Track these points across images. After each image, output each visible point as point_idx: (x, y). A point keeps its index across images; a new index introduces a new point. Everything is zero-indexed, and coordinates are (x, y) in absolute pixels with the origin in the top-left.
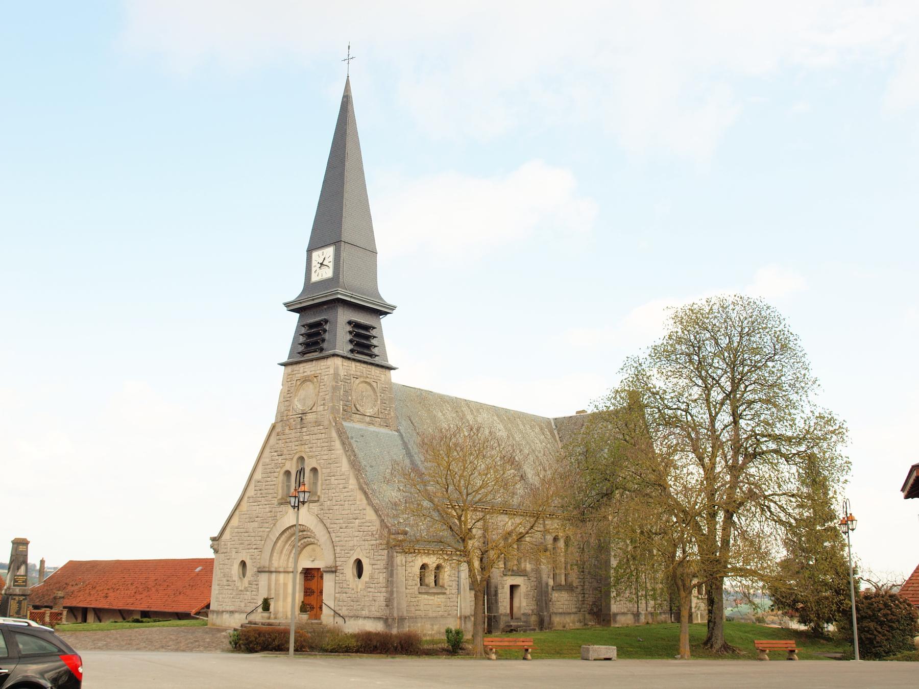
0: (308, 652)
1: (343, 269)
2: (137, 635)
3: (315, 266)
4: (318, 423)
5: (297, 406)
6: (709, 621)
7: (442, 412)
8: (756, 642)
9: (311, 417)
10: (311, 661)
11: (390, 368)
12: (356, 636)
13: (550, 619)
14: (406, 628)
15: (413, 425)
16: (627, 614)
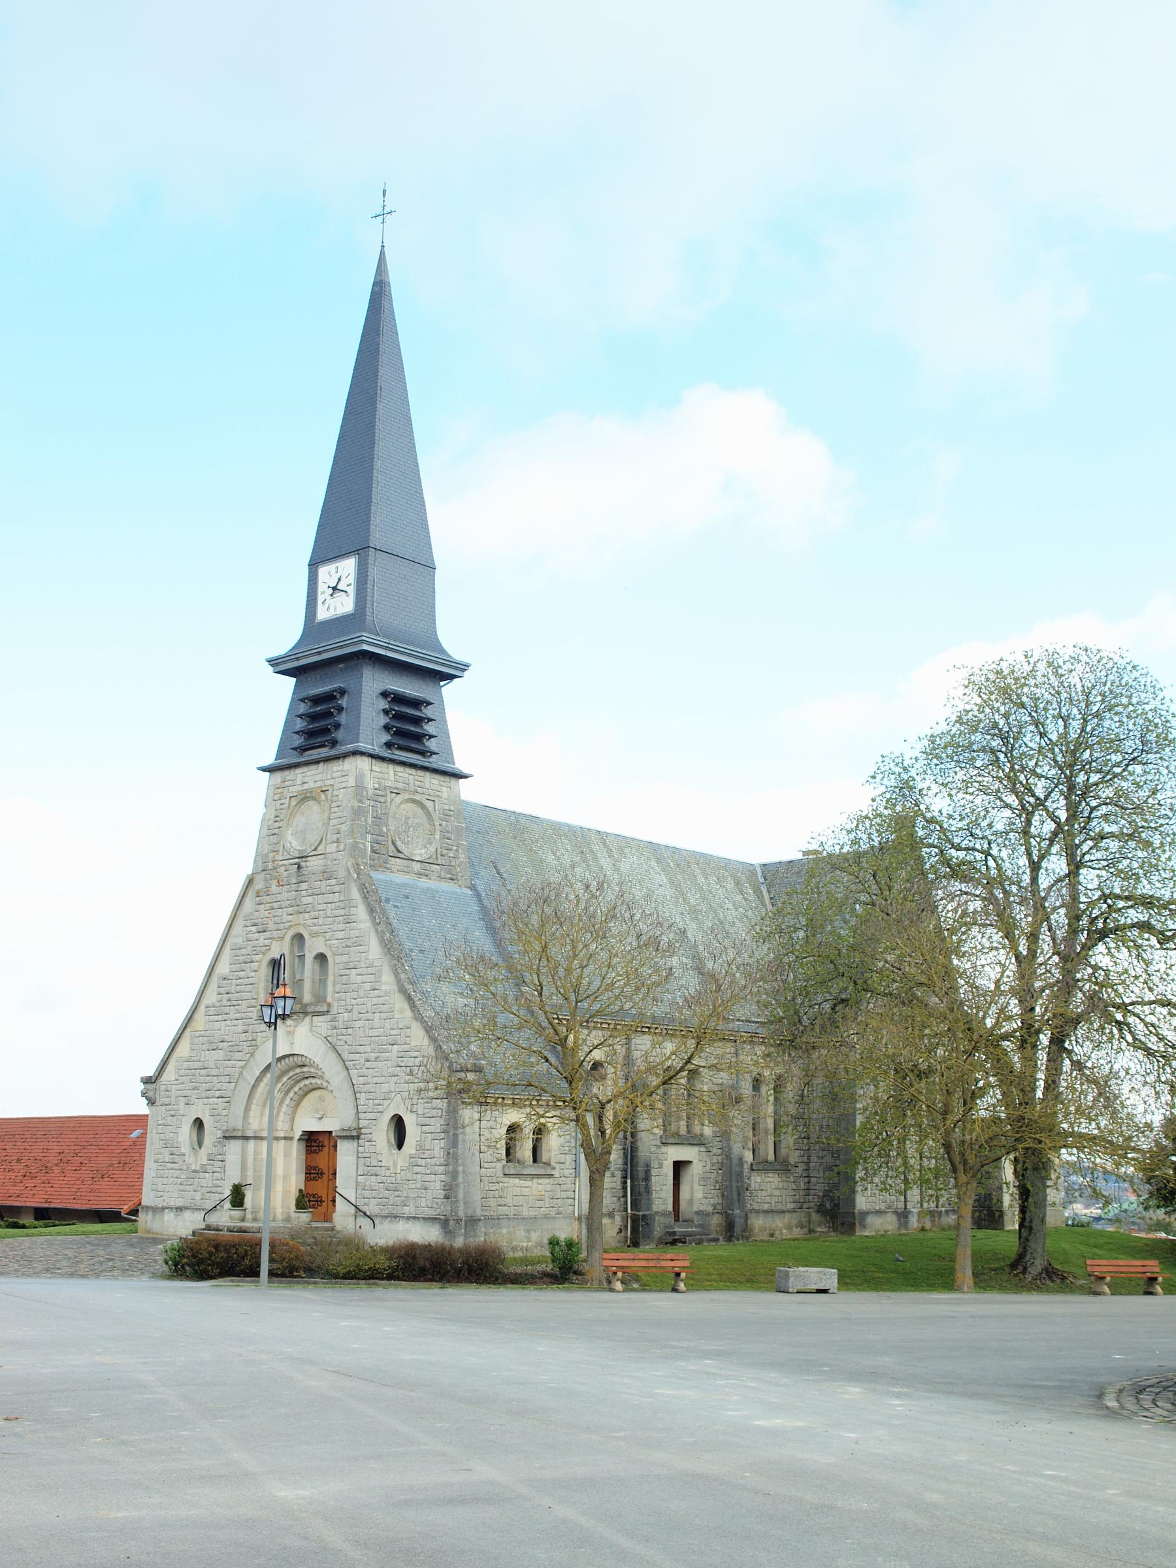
0: (303, 1278)
1: (373, 597)
3: (323, 593)
4: (327, 875)
5: (290, 843)
6: (1021, 1226)
8: (1088, 1262)
9: (316, 863)
10: (294, 1293)
11: (459, 776)
12: (389, 1251)
14: (481, 1237)
15: (501, 876)
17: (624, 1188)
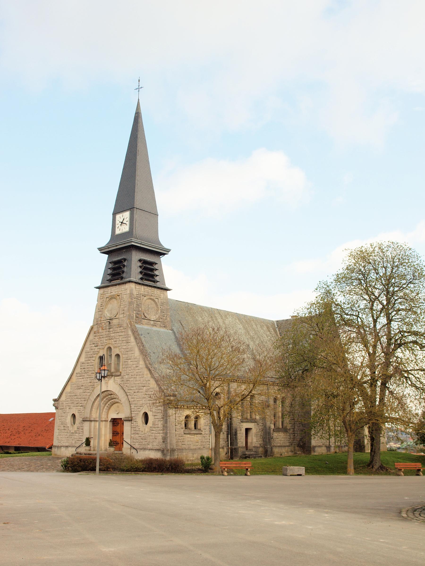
0: (112, 471)
2: (5, 462)
4: (120, 326)
5: (106, 314)
7: (201, 317)
11: (167, 290)
12: (142, 461)
13: (272, 450)
14: (176, 456)
16: (322, 446)
17: (228, 438)
